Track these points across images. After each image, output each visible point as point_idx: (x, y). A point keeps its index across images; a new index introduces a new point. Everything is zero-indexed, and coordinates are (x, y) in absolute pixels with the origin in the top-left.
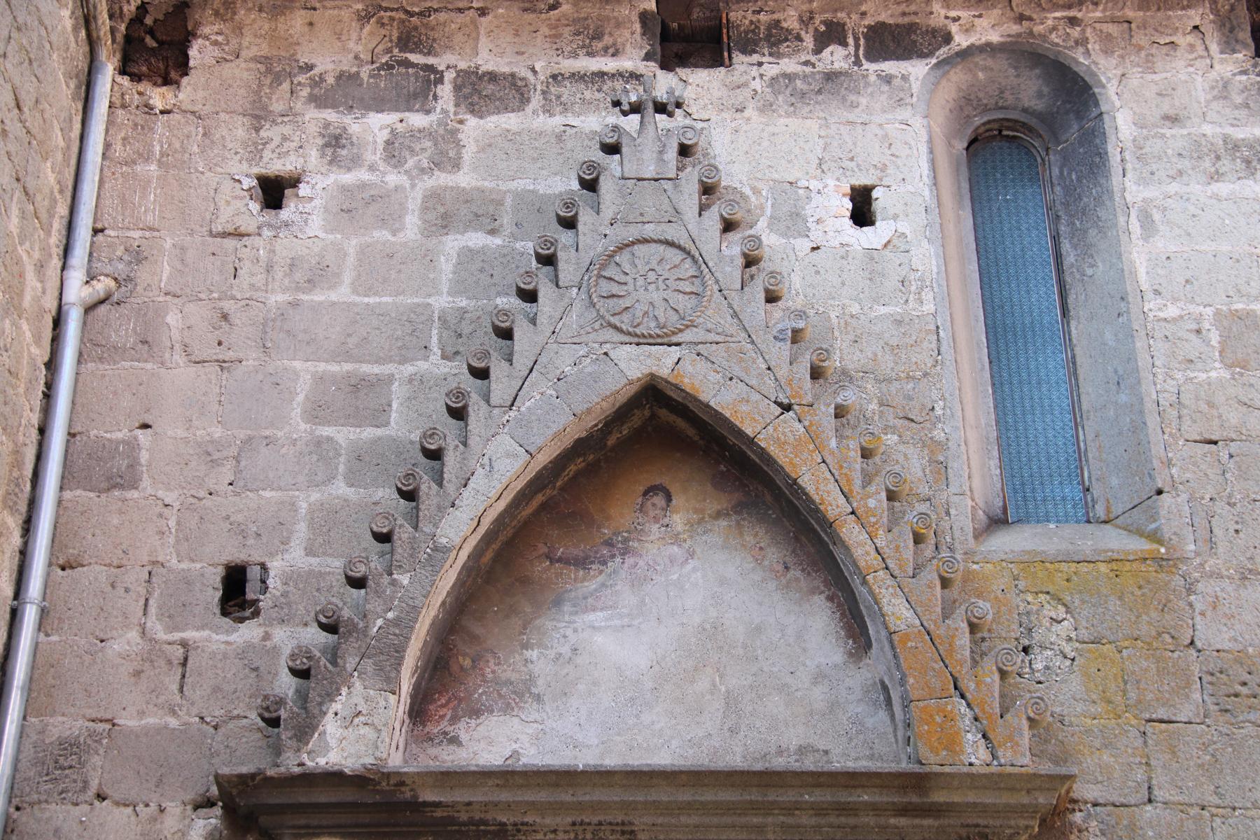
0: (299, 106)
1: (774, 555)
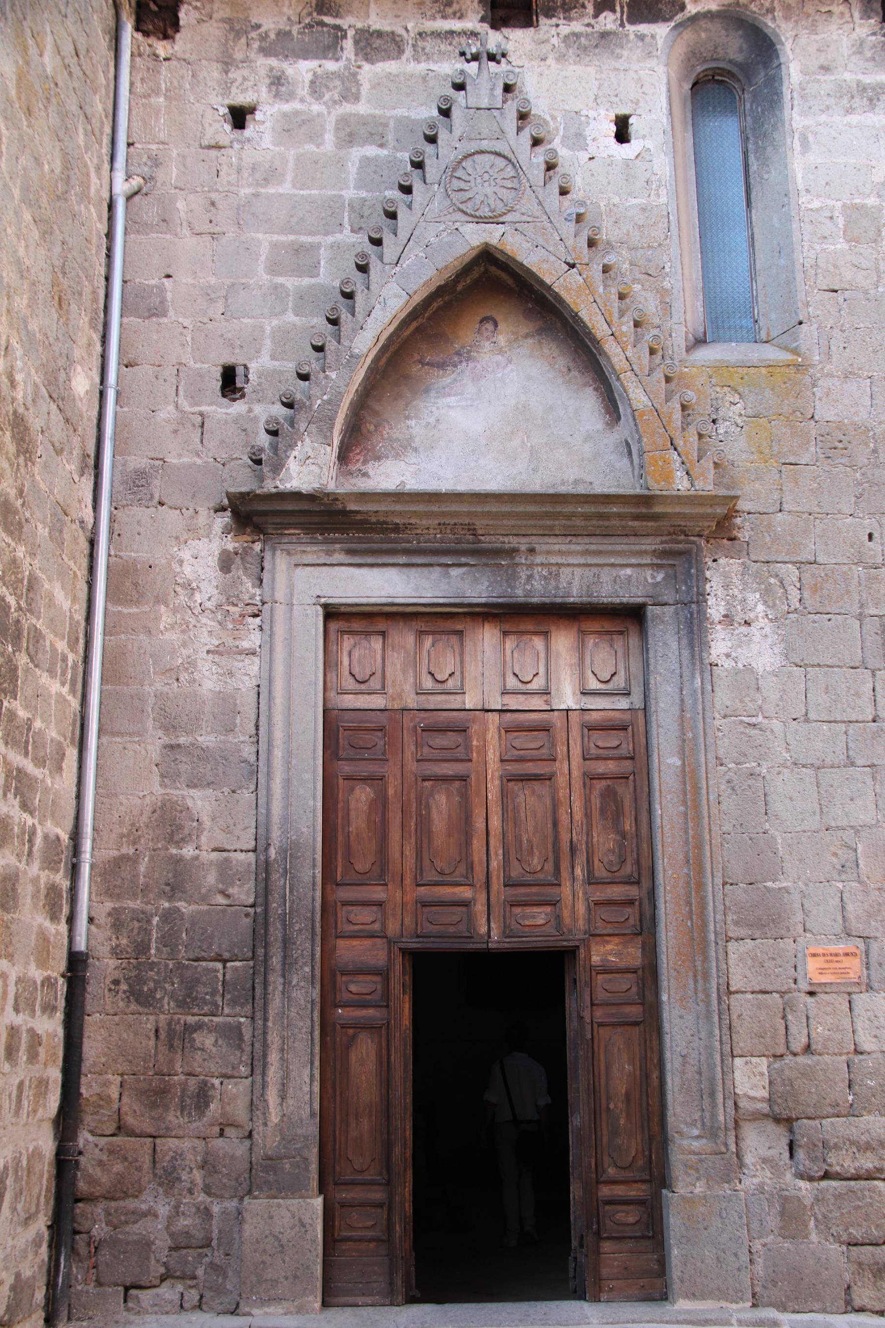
0: (252, 55)
1: (562, 362)
